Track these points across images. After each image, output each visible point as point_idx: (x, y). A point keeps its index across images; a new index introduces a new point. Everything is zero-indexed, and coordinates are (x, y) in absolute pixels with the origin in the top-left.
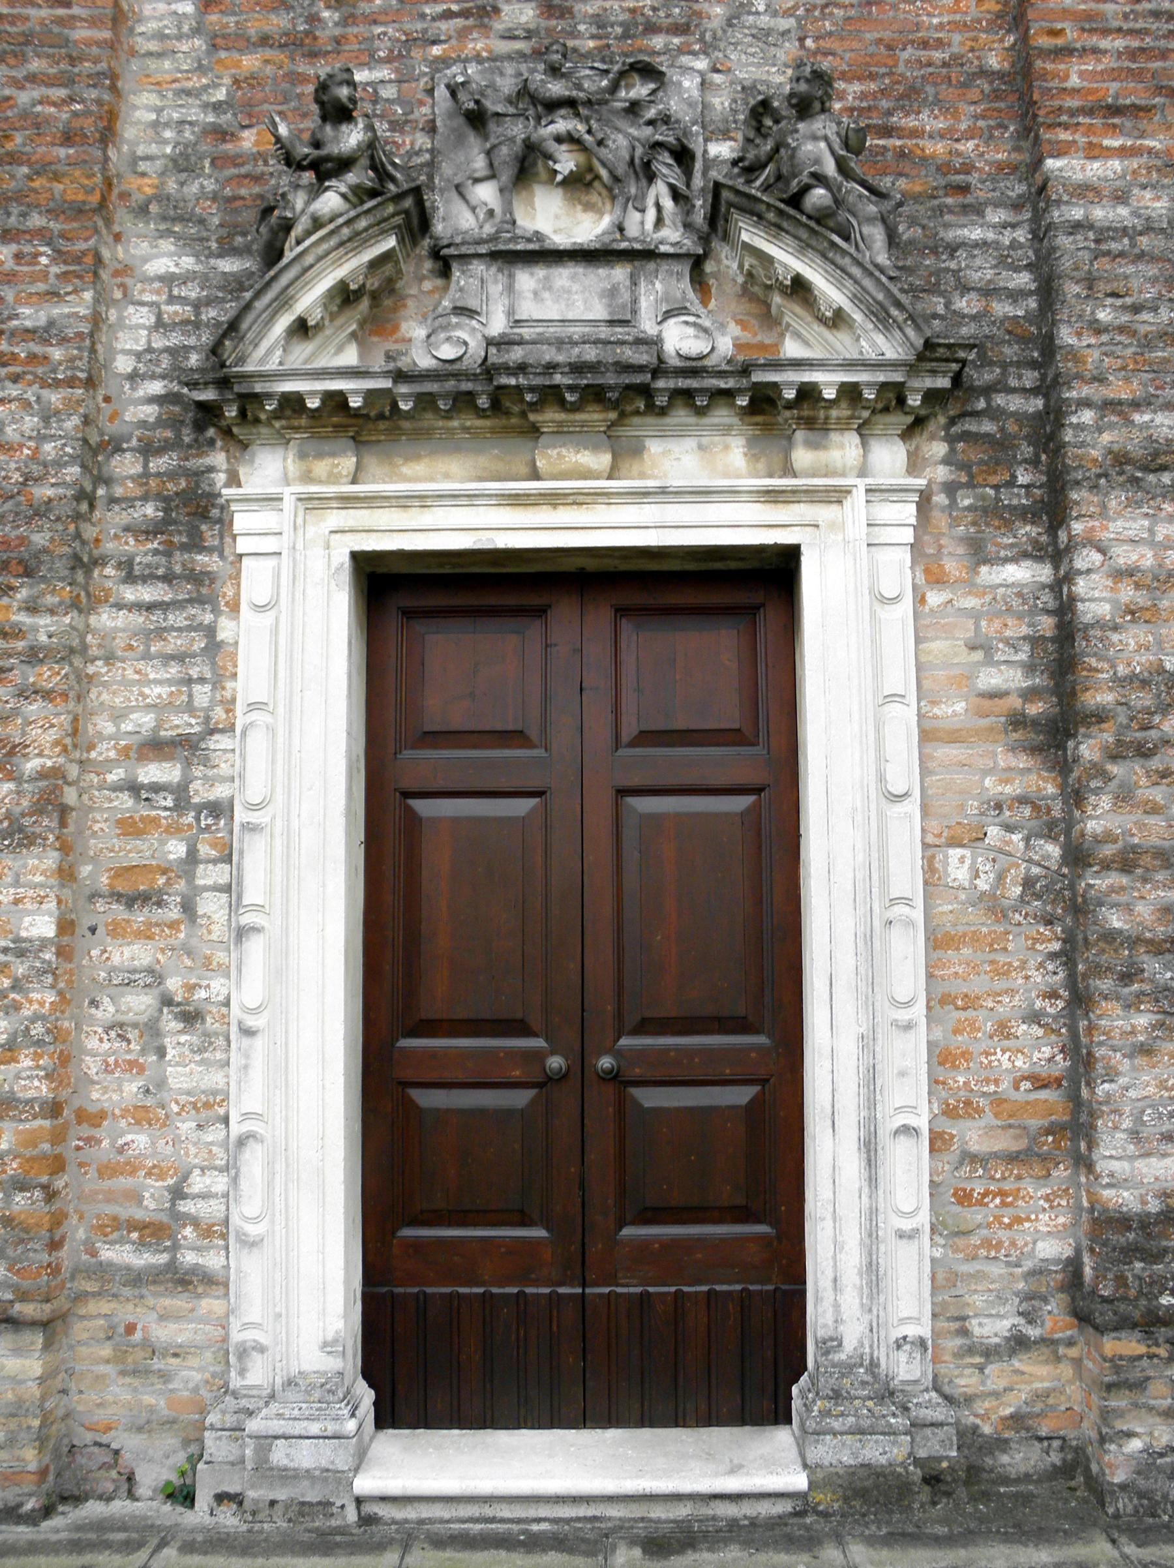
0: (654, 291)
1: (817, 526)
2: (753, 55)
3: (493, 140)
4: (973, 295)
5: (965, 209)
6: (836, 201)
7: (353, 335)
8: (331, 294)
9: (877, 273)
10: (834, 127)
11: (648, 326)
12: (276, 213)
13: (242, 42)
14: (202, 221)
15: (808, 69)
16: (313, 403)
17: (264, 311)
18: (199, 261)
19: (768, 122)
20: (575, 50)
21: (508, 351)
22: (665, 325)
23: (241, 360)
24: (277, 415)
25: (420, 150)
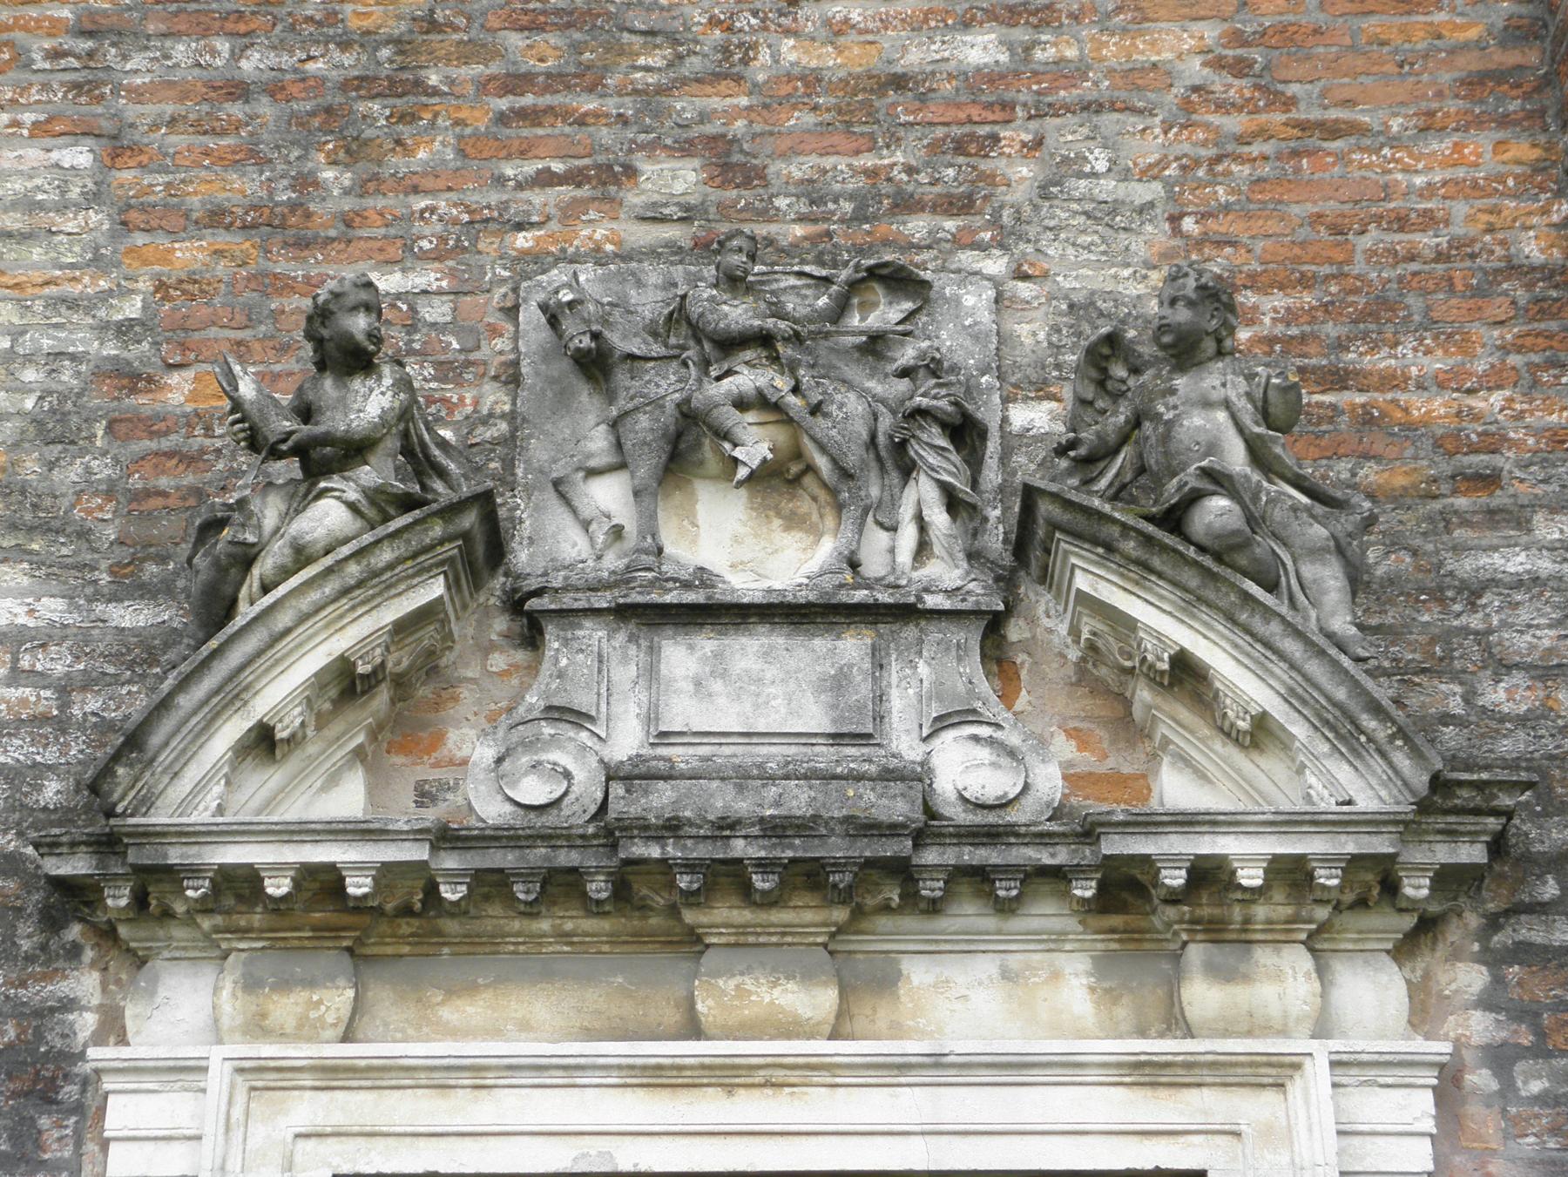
0: (918, 678)
1: (1237, 1134)
2: (1088, 248)
3: (623, 403)
4: (1518, 678)
5: (1493, 517)
6: (1251, 520)
7: (359, 754)
8: (320, 681)
9: (1333, 651)
10: (1242, 385)
11: (904, 744)
12: (227, 533)
13: (174, 218)
14: (83, 534)
15: (1191, 283)
16: (277, 887)
17: (195, 712)
18: (73, 607)
19: (1119, 371)
20: (770, 242)
21: (646, 792)
22: (936, 743)
23: (146, 802)
24: (205, 906)
25: (491, 415)
